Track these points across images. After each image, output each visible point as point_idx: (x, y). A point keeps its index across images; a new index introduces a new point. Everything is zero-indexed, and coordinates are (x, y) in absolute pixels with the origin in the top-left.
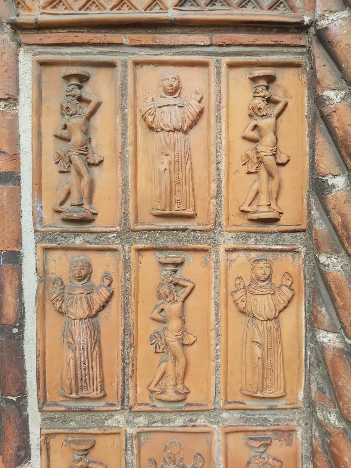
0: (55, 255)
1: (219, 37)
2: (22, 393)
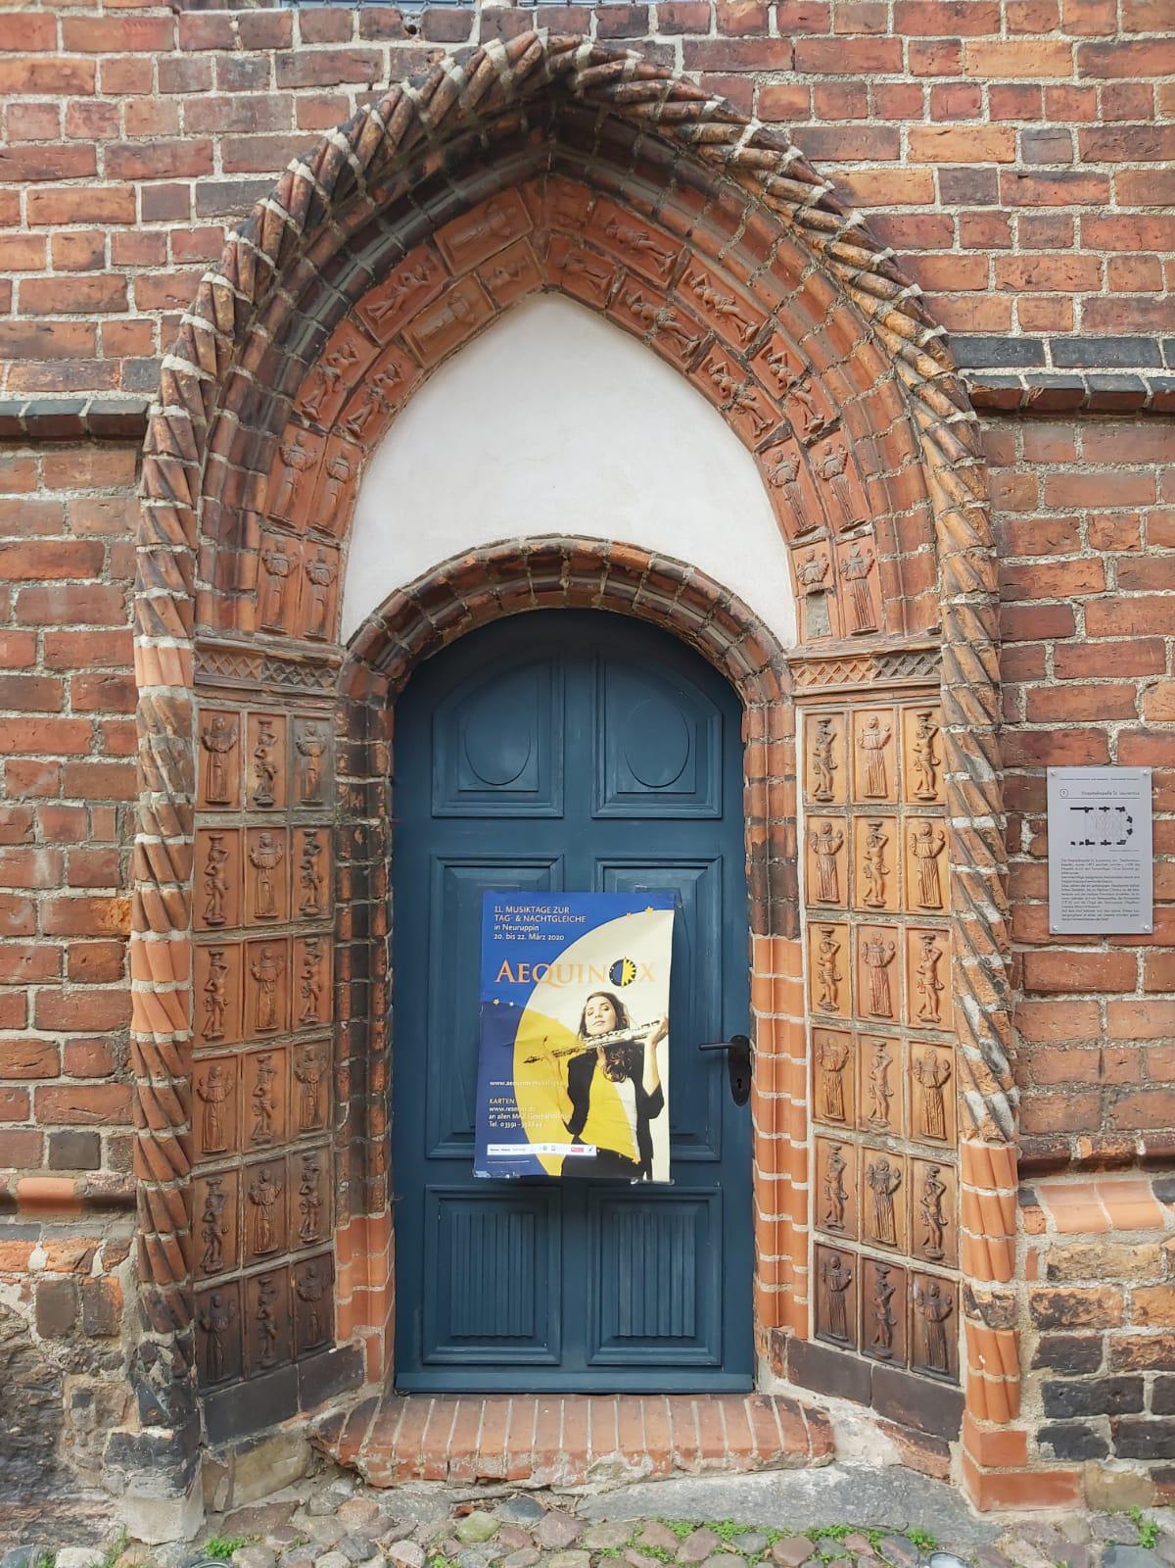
0: (813, 820)
1: (898, 694)
2: (797, 898)
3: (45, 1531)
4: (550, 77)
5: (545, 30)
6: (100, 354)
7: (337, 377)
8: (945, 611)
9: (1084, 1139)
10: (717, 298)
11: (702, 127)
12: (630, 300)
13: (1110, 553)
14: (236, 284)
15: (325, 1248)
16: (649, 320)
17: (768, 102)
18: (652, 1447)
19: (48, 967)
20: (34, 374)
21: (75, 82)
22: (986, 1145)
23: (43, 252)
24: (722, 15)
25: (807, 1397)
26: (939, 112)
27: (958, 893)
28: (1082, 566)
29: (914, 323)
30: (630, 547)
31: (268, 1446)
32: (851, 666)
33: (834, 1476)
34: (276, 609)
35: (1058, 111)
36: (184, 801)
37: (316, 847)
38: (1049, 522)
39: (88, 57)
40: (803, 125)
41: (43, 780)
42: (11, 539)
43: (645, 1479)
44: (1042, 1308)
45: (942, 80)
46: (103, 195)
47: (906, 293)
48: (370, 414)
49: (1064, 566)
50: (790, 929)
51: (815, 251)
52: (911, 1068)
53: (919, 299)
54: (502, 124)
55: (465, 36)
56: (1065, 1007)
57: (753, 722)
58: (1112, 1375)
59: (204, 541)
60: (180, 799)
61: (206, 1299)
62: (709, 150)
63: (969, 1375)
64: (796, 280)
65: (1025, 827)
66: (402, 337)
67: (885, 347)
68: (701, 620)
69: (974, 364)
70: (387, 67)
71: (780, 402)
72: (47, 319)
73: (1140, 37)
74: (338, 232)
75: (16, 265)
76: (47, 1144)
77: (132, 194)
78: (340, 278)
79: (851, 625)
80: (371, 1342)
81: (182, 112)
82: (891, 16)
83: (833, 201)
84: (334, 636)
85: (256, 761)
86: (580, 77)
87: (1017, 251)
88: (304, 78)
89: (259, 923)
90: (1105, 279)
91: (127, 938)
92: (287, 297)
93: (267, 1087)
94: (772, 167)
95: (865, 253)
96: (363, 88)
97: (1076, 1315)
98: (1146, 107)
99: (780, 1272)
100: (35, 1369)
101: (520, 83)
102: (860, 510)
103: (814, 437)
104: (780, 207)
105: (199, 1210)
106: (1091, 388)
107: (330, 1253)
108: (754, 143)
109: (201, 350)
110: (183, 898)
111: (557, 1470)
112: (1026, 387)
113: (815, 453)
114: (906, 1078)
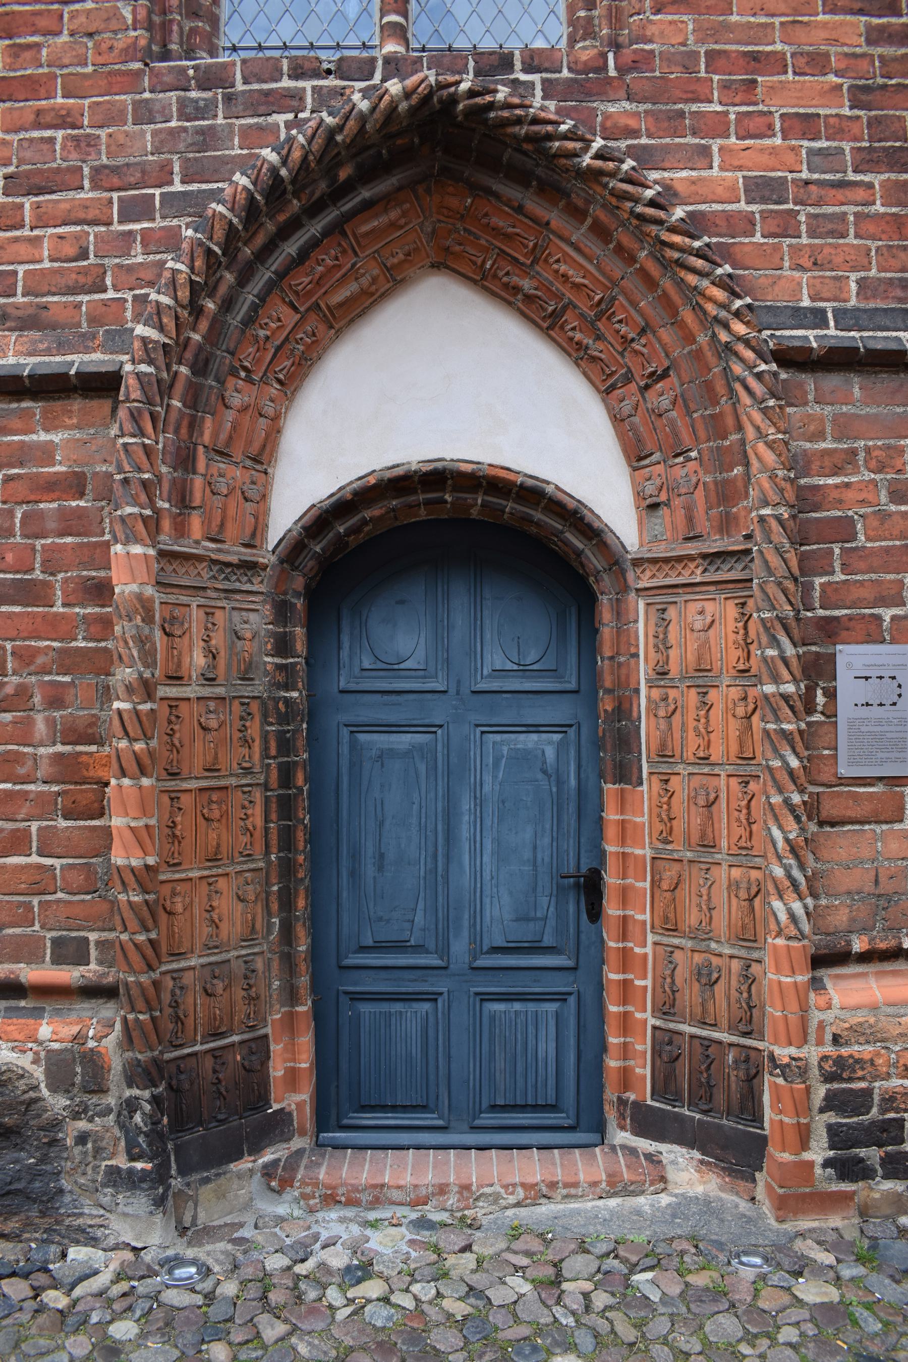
1: (719, 587)
3: (59, 1235)
4: (438, 106)
5: (433, 71)
6: (85, 325)
7: (267, 338)
8: (756, 520)
9: (863, 937)
10: (571, 273)
11: (557, 144)
12: (501, 274)
13: (882, 476)
14: (192, 268)
15: (262, 1032)
16: (516, 289)
17: (609, 124)
18: (523, 1180)
19: (44, 807)
20: (34, 342)
21: (69, 120)
22: (786, 942)
23: (42, 248)
24: (572, 59)
25: (645, 1145)
26: (742, 133)
27: (768, 746)
28: (862, 486)
29: (726, 294)
30: (503, 468)
31: (222, 1180)
32: (683, 565)
33: (665, 1200)
34: (219, 523)
35: (835, 133)
36: (149, 676)
37: (249, 714)
38: (836, 450)
39: (79, 101)
40: (636, 142)
41: (40, 660)
42: (16, 471)
43: (518, 1205)
44: (827, 1066)
45: (744, 109)
46: (88, 203)
47: (719, 271)
48: (292, 365)
49: (847, 485)
50: (634, 779)
51: (648, 239)
52: (729, 886)
53: (730, 276)
54: (399, 142)
55: (370, 76)
56: (850, 834)
57: (606, 614)
58: (881, 1117)
59: (164, 469)
60: (147, 675)
61: (173, 1068)
62: (563, 161)
63: (771, 1119)
64: (632, 259)
65: (819, 692)
66: (318, 305)
67: (705, 312)
68: (560, 527)
69: (774, 326)
70: (309, 100)
71: (622, 354)
72: (44, 299)
73: (893, 82)
74: (270, 227)
75: (20, 259)
76: (49, 944)
77: (110, 201)
78: (270, 261)
79: (682, 532)
80: (300, 1105)
81: (149, 137)
82: (703, 59)
83: (662, 201)
84: (262, 544)
85: (202, 644)
86: (461, 106)
87: (805, 240)
88: (244, 110)
89: (207, 774)
90: (874, 262)
91: (107, 784)
92: (229, 277)
93: (215, 904)
94: (612, 174)
95: (687, 240)
96: (290, 116)
97: (854, 1071)
98: (901, 132)
99: (625, 1051)
100: (46, 1116)
101: (413, 111)
102: (686, 438)
103: (650, 381)
104: (620, 204)
105: (166, 998)
106: (864, 347)
107: (266, 1036)
108: (597, 156)
109: (165, 320)
110: (151, 753)
111: (448, 1199)
112: (815, 345)
113: (650, 395)
114: (726, 894)
